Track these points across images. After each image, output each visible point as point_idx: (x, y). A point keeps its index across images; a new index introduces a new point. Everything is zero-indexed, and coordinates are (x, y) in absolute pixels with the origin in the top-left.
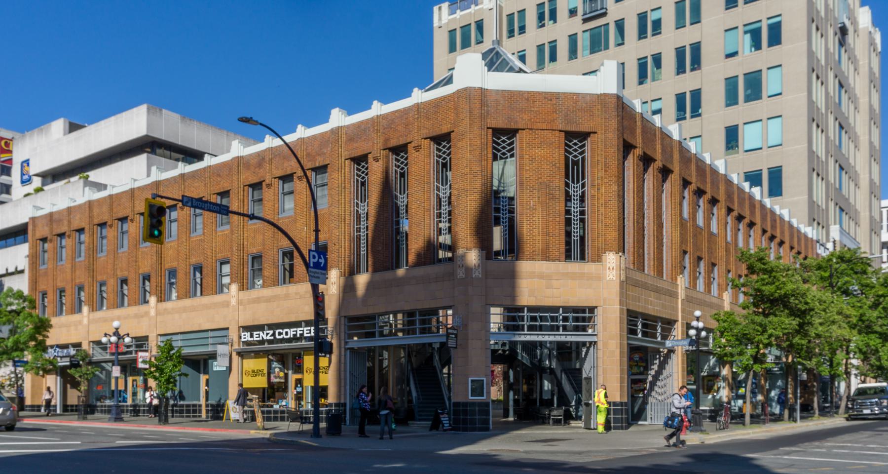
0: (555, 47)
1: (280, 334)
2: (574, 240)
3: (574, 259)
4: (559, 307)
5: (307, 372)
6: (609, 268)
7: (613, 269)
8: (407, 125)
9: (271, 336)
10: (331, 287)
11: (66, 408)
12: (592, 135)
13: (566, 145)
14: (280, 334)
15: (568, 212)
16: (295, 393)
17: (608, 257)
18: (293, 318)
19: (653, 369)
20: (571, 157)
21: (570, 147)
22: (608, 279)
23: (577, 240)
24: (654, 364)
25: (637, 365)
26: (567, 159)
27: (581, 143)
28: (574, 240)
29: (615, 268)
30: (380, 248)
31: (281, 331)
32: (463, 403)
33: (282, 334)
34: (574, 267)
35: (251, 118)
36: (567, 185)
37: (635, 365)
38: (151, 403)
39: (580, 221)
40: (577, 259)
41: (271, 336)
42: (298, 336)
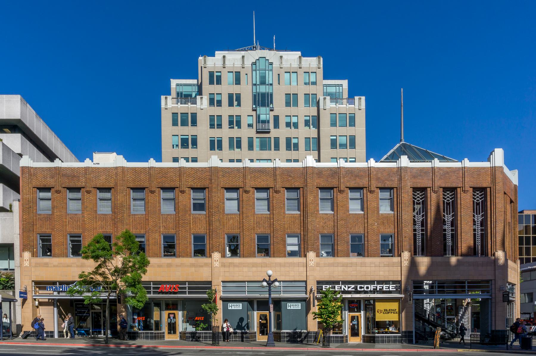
0: (240, 141)
1: (361, 288)
2: (448, 245)
3: (418, 255)
4: (151, 282)
5: (378, 312)
6: (215, 261)
7: (217, 261)
8: (479, 175)
9: (344, 288)
10: (310, 262)
11: (61, 334)
12: (82, 189)
13: (474, 195)
14: (361, 288)
15: (415, 230)
16: (351, 325)
17: (25, 254)
18: (369, 279)
19: (460, 313)
20: (446, 201)
21: (475, 196)
22: (25, 266)
23: (420, 245)
24: (460, 311)
25: (450, 311)
26: (474, 202)
27: (481, 193)
28: (448, 245)
29: (28, 260)
30: (438, 243)
31: (363, 286)
32: (502, 330)
33: (363, 288)
34: (46, 260)
35: (22, 157)
36: (474, 216)
37: (449, 312)
38: (228, 331)
39: (451, 235)
40: (420, 255)
41: (344, 288)
42: (378, 289)
